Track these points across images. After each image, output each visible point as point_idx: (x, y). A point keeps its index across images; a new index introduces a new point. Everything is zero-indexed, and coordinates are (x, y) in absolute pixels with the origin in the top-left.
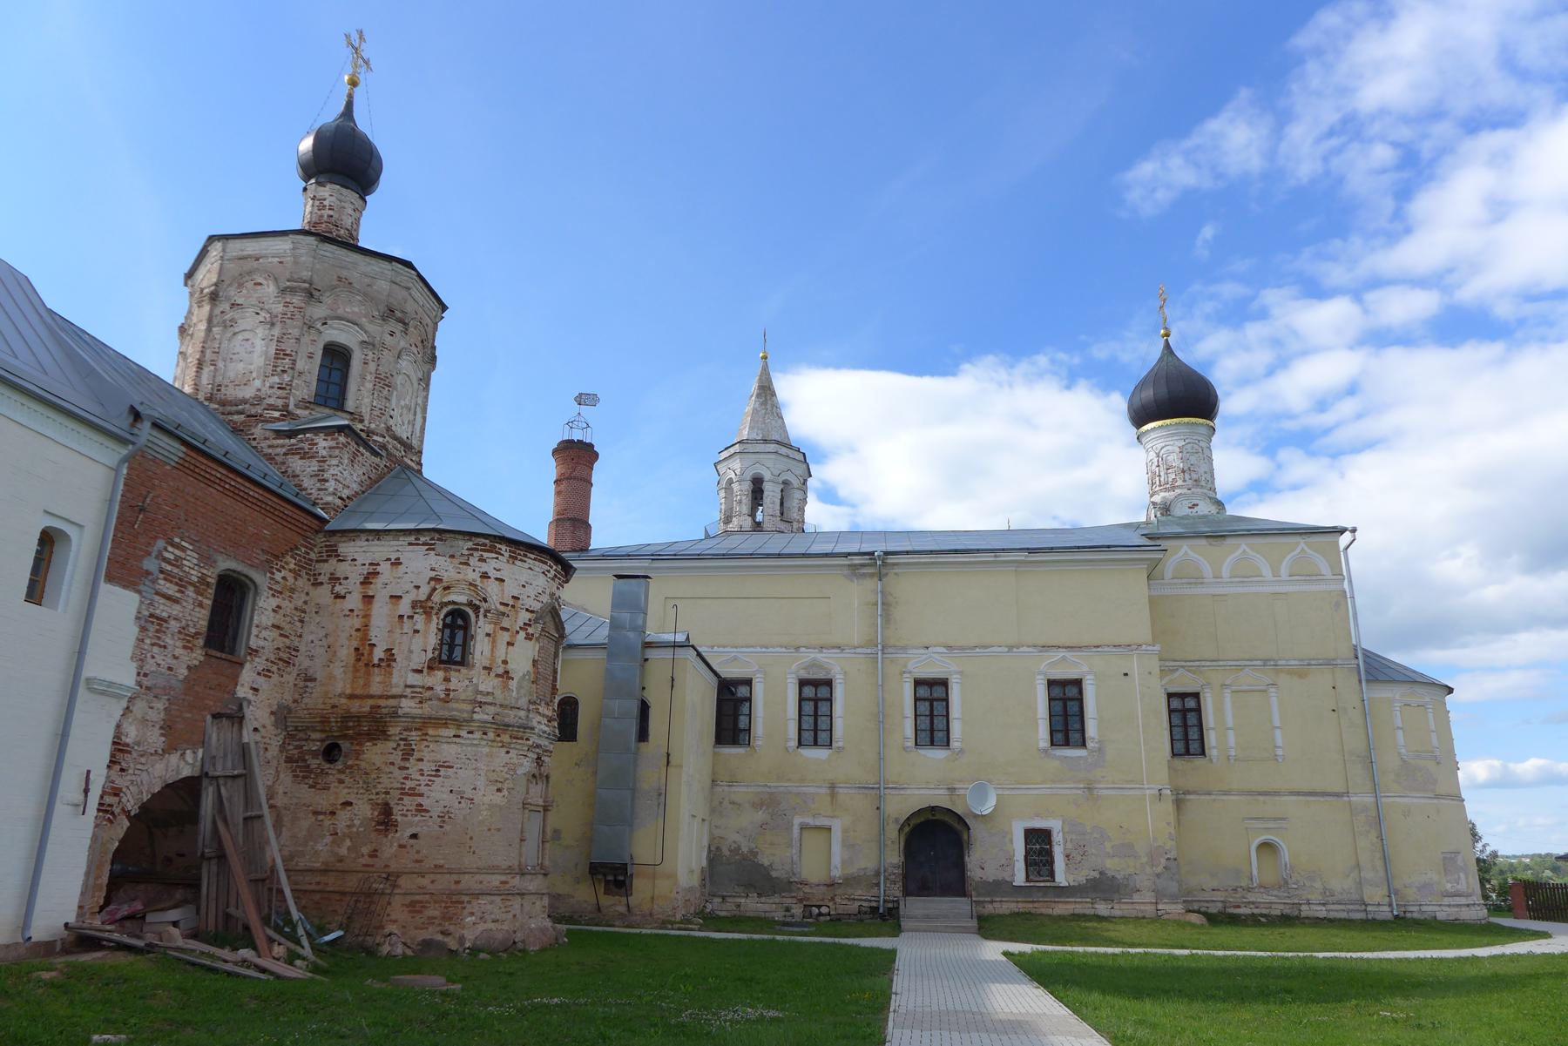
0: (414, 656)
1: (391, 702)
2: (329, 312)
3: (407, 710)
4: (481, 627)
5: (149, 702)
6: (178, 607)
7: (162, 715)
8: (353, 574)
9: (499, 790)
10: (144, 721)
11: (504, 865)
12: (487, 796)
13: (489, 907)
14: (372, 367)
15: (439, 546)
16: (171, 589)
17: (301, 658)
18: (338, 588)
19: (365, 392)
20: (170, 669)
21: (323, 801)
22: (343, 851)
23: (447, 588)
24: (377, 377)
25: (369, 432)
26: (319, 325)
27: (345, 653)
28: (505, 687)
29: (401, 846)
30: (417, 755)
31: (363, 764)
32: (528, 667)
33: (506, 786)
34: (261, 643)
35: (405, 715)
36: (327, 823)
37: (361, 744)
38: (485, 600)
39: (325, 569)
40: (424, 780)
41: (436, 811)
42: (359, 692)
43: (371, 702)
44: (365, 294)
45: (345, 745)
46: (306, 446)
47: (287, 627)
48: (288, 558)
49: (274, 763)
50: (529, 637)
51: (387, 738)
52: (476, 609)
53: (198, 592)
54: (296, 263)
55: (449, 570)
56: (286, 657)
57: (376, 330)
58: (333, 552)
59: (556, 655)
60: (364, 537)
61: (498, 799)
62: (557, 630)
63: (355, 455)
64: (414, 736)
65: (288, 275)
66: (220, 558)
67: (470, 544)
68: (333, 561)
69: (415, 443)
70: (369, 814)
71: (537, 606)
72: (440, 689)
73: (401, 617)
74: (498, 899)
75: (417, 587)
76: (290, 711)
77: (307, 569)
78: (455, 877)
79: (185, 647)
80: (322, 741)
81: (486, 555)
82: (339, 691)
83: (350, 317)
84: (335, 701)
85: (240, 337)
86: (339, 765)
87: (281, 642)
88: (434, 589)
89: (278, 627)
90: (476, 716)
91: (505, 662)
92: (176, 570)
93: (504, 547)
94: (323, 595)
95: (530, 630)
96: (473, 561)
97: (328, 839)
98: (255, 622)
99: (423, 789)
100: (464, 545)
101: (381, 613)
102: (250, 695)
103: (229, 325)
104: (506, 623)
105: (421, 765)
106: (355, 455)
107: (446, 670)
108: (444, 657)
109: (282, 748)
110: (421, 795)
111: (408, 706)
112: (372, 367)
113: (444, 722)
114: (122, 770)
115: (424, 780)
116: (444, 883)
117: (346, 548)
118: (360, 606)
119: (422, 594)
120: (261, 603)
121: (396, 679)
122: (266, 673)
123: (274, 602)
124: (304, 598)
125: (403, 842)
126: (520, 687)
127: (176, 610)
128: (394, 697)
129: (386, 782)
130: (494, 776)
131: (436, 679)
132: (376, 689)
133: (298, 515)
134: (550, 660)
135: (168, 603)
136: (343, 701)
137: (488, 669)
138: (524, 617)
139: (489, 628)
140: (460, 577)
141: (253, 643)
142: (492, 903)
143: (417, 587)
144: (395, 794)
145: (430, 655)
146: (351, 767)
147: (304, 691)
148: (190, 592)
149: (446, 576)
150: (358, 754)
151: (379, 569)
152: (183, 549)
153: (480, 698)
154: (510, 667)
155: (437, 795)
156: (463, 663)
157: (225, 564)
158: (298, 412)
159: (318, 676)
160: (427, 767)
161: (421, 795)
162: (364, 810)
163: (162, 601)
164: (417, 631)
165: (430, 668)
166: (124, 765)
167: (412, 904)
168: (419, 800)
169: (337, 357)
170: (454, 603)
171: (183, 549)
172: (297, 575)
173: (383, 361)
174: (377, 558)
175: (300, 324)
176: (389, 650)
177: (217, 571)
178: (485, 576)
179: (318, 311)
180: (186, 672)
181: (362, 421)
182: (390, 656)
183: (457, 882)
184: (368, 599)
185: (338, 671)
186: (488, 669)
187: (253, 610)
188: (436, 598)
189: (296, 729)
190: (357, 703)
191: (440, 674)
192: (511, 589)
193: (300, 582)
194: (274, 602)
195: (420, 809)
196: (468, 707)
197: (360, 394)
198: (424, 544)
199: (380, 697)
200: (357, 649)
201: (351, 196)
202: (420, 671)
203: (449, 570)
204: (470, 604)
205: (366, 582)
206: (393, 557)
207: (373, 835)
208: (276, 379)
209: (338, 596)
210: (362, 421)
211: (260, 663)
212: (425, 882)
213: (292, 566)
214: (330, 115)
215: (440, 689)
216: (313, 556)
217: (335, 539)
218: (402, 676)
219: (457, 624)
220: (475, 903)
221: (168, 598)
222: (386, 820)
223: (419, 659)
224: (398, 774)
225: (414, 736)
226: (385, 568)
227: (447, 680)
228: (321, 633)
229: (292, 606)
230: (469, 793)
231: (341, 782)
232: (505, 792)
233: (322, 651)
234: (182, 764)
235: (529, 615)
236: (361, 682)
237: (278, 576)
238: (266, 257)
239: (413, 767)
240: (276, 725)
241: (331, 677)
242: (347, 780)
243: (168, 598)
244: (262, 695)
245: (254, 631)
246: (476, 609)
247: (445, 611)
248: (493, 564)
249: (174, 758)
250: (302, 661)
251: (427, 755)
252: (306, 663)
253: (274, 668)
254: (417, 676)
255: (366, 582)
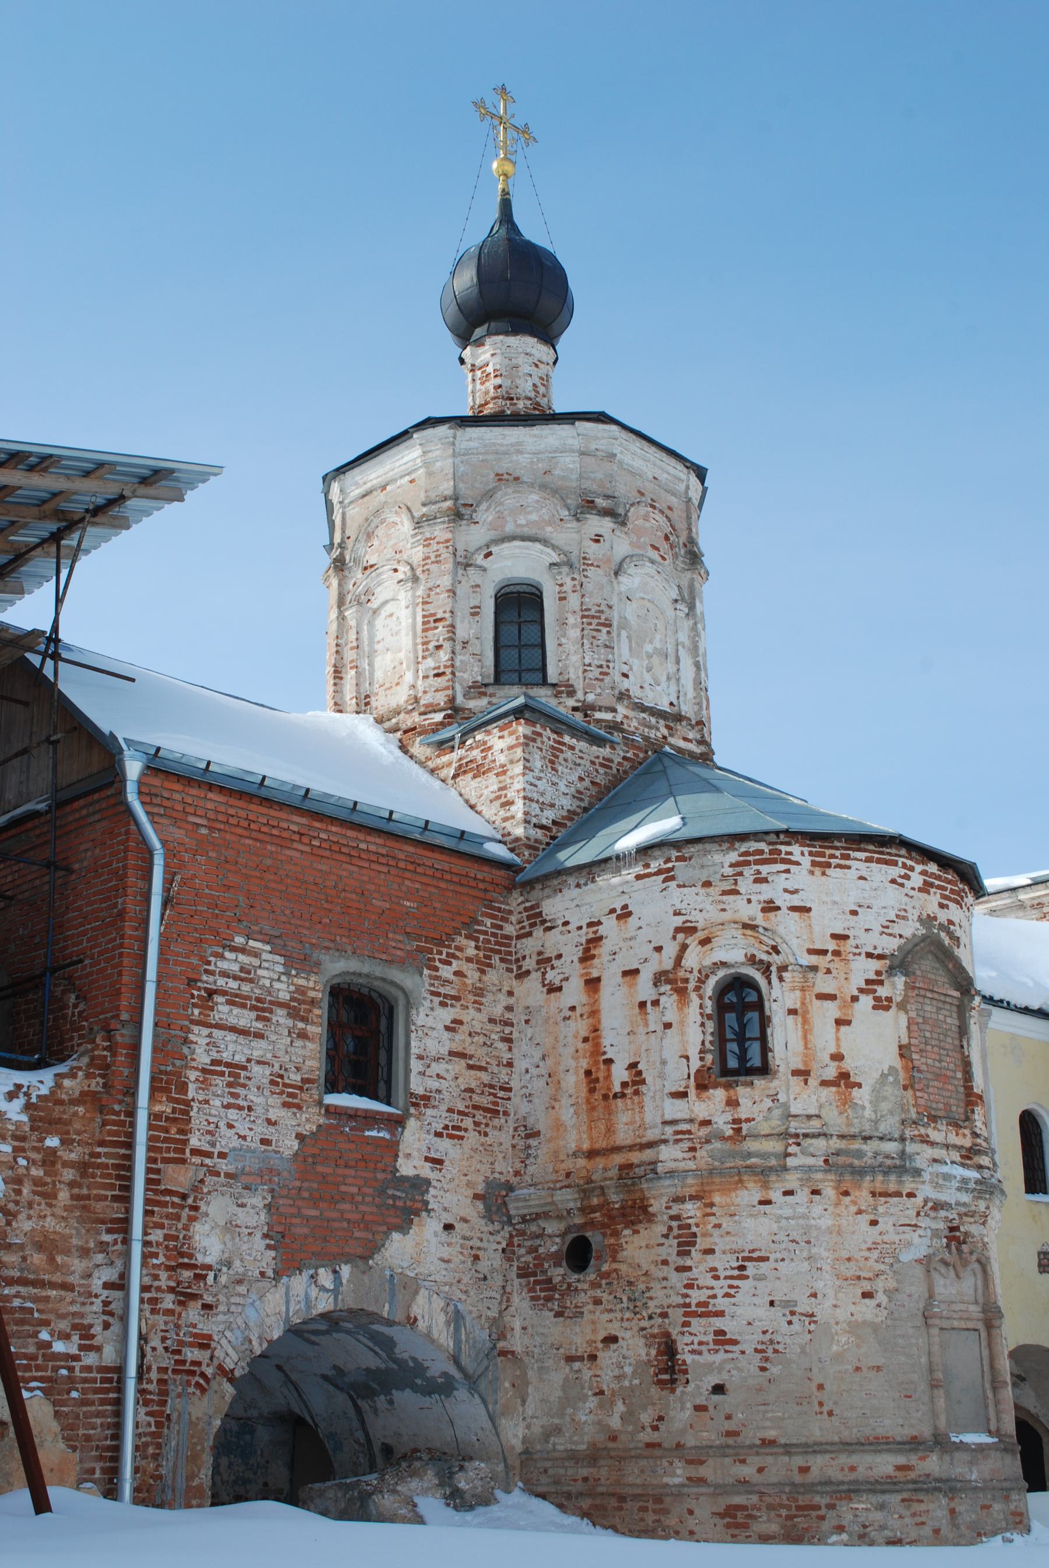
0: (669, 1068)
1: (648, 1155)
2: (493, 534)
3: (672, 1165)
4: (780, 997)
5: (235, 1197)
6: (262, 1043)
7: (263, 1216)
8: (566, 944)
9: (867, 1295)
10: (231, 1227)
11: (907, 1432)
12: (840, 1307)
13: (877, 1516)
14: (574, 601)
15: (681, 870)
16: (244, 1018)
17: (516, 1100)
18: (550, 975)
19: (571, 647)
20: (265, 1142)
21: (579, 1336)
22: (615, 1422)
23: (705, 942)
24: (586, 615)
25: (585, 709)
26: (479, 559)
27: (573, 1081)
28: (846, 1102)
29: (698, 1408)
30: (701, 1243)
31: (624, 1268)
32: (891, 1058)
33: (880, 1285)
34: (434, 1084)
35: (671, 1173)
36: (587, 1374)
37: (616, 1234)
38: (776, 950)
39: (529, 946)
40: (721, 1286)
41: (750, 1341)
42: (601, 1144)
43: (618, 1159)
44: (543, 487)
45: (594, 1237)
46: (476, 753)
47: (481, 1052)
48: (461, 941)
49: (499, 1281)
50: (882, 1005)
51: (650, 1218)
52: (766, 969)
53: (294, 1014)
54: (430, 474)
55: (702, 907)
56: (488, 1105)
57: (570, 536)
58: (536, 918)
59: (963, 1031)
60: (572, 881)
61: (867, 1310)
62: (958, 987)
63: (556, 750)
64: (690, 1209)
65: (422, 497)
66: (324, 958)
67: (733, 857)
68: (538, 932)
69: (687, 709)
70: (643, 1352)
71: (889, 945)
72: (722, 1121)
73: (642, 1005)
74: (894, 1499)
75: (659, 949)
76: (510, 1188)
77: (499, 951)
78: (799, 1461)
79: (285, 1105)
80: (563, 1235)
81: (765, 869)
82: (573, 1146)
83: (526, 531)
84: (569, 1165)
85: (384, 613)
86: (591, 1275)
87: (472, 1079)
88: (684, 947)
89: (462, 1055)
90: (790, 1162)
91: (838, 1057)
92: (246, 988)
93: (796, 849)
94: (531, 991)
95: (882, 992)
96: (745, 885)
97: (592, 1402)
98: (414, 1051)
99: (721, 1303)
100: (725, 859)
101: (615, 1003)
102: (426, 1171)
103: (363, 600)
104: (824, 984)
105: (711, 1261)
106: (556, 750)
107: (728, 1086)
108: (733, 1063)
109: (508, 1253)
110: (720, 1314)
111: (670, 1155)
112: (574, 601)
113: (737, 1178)
114: (207, 1307)
115: (721, 1286)
116: (779, 1469)
117: (554, 907)
118: (584, 998)
119: (667, 960)
120: (420, 1018)
121: (651, 1115)
122: (452, 1133)
123: (446, 1015)
124: (504, 1000)
125: (700, 1401)
126: (877, 1098)
127: (259, 1049)
128: (651, 1145)
129: (659, 1297)
130: (851, 1269)
131: (712, 1105)
132: (623, 1136)
133: (459, 866)
134: (950, 1042)
135: (241, 1039)
136: (582, 1162)
137: (803, 1074)
138: (864, 969)
139: (792, 1000)
140: (727, 916)
141: (417, 1086)
142: (881, 1507)
143: (659, 949)
144: (677, 1315)
145: (695, 1064)
146: (607, 1275)
147: (526, 1156)
148: (280, 1016)
149: (699, 920)
150: (614, 1252)
151: (602, 930)
152: (256, 954)
153: (794, 1126)
154: (848, 1065)
155: (747, 1312)
156: (764, 1070)
157: (338, 966)
158: (472, 704)
159: (541, 1126)
160: (724, 1263)
161: (720, 1314)
162: (635, 1349)
163: (231, 1037)
164: (668, 1026)
165: (702, 1087)
166: (209, 1299)
167: (730, 1511)
168: (718, 1323)
169: (519, 605)
170: (724, 964)
171: (256, 954)
172: (483, 966)
173: (589, 587)
174: (597, 911)
175: (449, 566)
176: (633, 1066)
177: (324, 978)
178: (770, 907)
179: (474, 536)
180: (295, 1145)
181: (571, 693)
182: (637, 1078)
183: (804, 1470)
184: (593, 984)
185: (567, 1114)
186: (803, 1074)
187: (408, 1033)
188: (693, 959)
189: (524, 1220)
190: (600, 1162)
191: (719, 1095)
192: (826, 922)
193: (492, 977)
194: (446, 1015)
195: (722, 1339)
196: (774, 1146)
197: (566, 652)
198: (659, 873)
199: (631, 1148)
200: (588, 1073)
201: (528, 344)
202: (684, 1095)
203: (702, 907)
204: (752, 960)
205: (587, 957)
206: (618, 906)
207: (655, 1391)
208: (430, 663)
209: (554, 989)
210: (571, 693)
211: (437, 1117)
212: (747, 1471)
213: (471, 952)
214: (480, 226)
215: (722, 1121)
216: (510, 929)
217: (536, 893)
218: (657, 1109)
219: (739, 1003)
220: (843, 1507)
221: (243, 1032)
222: (669, 1366)
223: (677, 1075)
224: (677, 1280)
225: (690, 1209)
226: (609, 927)
227: (732, 1103)
228: (537, 1054)
229: (483, 1017)
230: (805, 1305)
231: (597, 1302)
232: (881, 1298)
233: (542, 1083)
234: (314, 1292)
235: (875, 965)
236: (602, 1127)
237: (446, 972)
238: (393, 481)
239: (699, 1266)
240: (488, 1216)
241: (559, 1126)
242: (605, 1297)
243: (243, 1032)
244: (450, 1170)
245: (415, 1065)
246: (766, 969)
247: (712, 982)
248: (781, 882)
249: (299, 1283)
250: (518, 1105)
251: (720, 1243)
252: (524, 1108)
253: (468, 1122)
254: (680, 1103)
255: (587, 957)
